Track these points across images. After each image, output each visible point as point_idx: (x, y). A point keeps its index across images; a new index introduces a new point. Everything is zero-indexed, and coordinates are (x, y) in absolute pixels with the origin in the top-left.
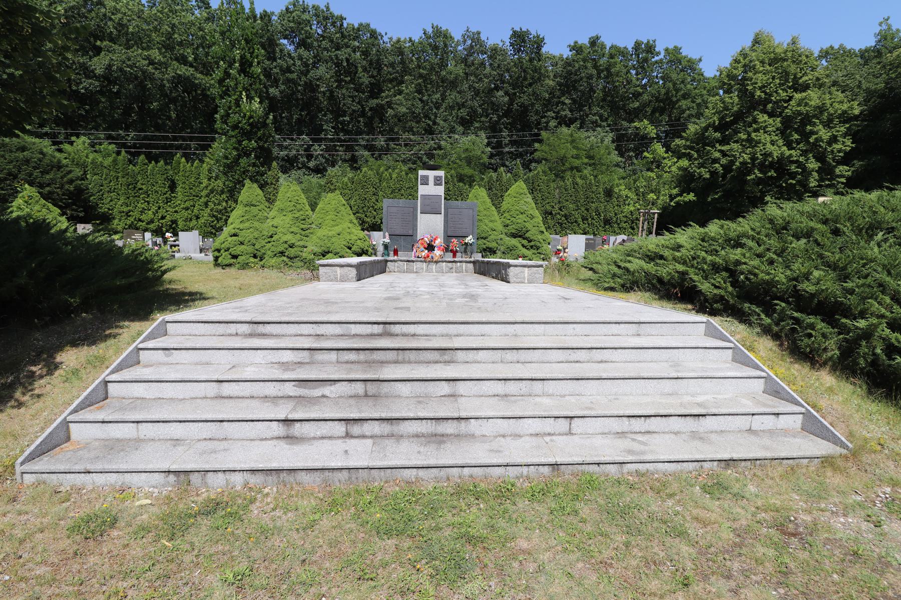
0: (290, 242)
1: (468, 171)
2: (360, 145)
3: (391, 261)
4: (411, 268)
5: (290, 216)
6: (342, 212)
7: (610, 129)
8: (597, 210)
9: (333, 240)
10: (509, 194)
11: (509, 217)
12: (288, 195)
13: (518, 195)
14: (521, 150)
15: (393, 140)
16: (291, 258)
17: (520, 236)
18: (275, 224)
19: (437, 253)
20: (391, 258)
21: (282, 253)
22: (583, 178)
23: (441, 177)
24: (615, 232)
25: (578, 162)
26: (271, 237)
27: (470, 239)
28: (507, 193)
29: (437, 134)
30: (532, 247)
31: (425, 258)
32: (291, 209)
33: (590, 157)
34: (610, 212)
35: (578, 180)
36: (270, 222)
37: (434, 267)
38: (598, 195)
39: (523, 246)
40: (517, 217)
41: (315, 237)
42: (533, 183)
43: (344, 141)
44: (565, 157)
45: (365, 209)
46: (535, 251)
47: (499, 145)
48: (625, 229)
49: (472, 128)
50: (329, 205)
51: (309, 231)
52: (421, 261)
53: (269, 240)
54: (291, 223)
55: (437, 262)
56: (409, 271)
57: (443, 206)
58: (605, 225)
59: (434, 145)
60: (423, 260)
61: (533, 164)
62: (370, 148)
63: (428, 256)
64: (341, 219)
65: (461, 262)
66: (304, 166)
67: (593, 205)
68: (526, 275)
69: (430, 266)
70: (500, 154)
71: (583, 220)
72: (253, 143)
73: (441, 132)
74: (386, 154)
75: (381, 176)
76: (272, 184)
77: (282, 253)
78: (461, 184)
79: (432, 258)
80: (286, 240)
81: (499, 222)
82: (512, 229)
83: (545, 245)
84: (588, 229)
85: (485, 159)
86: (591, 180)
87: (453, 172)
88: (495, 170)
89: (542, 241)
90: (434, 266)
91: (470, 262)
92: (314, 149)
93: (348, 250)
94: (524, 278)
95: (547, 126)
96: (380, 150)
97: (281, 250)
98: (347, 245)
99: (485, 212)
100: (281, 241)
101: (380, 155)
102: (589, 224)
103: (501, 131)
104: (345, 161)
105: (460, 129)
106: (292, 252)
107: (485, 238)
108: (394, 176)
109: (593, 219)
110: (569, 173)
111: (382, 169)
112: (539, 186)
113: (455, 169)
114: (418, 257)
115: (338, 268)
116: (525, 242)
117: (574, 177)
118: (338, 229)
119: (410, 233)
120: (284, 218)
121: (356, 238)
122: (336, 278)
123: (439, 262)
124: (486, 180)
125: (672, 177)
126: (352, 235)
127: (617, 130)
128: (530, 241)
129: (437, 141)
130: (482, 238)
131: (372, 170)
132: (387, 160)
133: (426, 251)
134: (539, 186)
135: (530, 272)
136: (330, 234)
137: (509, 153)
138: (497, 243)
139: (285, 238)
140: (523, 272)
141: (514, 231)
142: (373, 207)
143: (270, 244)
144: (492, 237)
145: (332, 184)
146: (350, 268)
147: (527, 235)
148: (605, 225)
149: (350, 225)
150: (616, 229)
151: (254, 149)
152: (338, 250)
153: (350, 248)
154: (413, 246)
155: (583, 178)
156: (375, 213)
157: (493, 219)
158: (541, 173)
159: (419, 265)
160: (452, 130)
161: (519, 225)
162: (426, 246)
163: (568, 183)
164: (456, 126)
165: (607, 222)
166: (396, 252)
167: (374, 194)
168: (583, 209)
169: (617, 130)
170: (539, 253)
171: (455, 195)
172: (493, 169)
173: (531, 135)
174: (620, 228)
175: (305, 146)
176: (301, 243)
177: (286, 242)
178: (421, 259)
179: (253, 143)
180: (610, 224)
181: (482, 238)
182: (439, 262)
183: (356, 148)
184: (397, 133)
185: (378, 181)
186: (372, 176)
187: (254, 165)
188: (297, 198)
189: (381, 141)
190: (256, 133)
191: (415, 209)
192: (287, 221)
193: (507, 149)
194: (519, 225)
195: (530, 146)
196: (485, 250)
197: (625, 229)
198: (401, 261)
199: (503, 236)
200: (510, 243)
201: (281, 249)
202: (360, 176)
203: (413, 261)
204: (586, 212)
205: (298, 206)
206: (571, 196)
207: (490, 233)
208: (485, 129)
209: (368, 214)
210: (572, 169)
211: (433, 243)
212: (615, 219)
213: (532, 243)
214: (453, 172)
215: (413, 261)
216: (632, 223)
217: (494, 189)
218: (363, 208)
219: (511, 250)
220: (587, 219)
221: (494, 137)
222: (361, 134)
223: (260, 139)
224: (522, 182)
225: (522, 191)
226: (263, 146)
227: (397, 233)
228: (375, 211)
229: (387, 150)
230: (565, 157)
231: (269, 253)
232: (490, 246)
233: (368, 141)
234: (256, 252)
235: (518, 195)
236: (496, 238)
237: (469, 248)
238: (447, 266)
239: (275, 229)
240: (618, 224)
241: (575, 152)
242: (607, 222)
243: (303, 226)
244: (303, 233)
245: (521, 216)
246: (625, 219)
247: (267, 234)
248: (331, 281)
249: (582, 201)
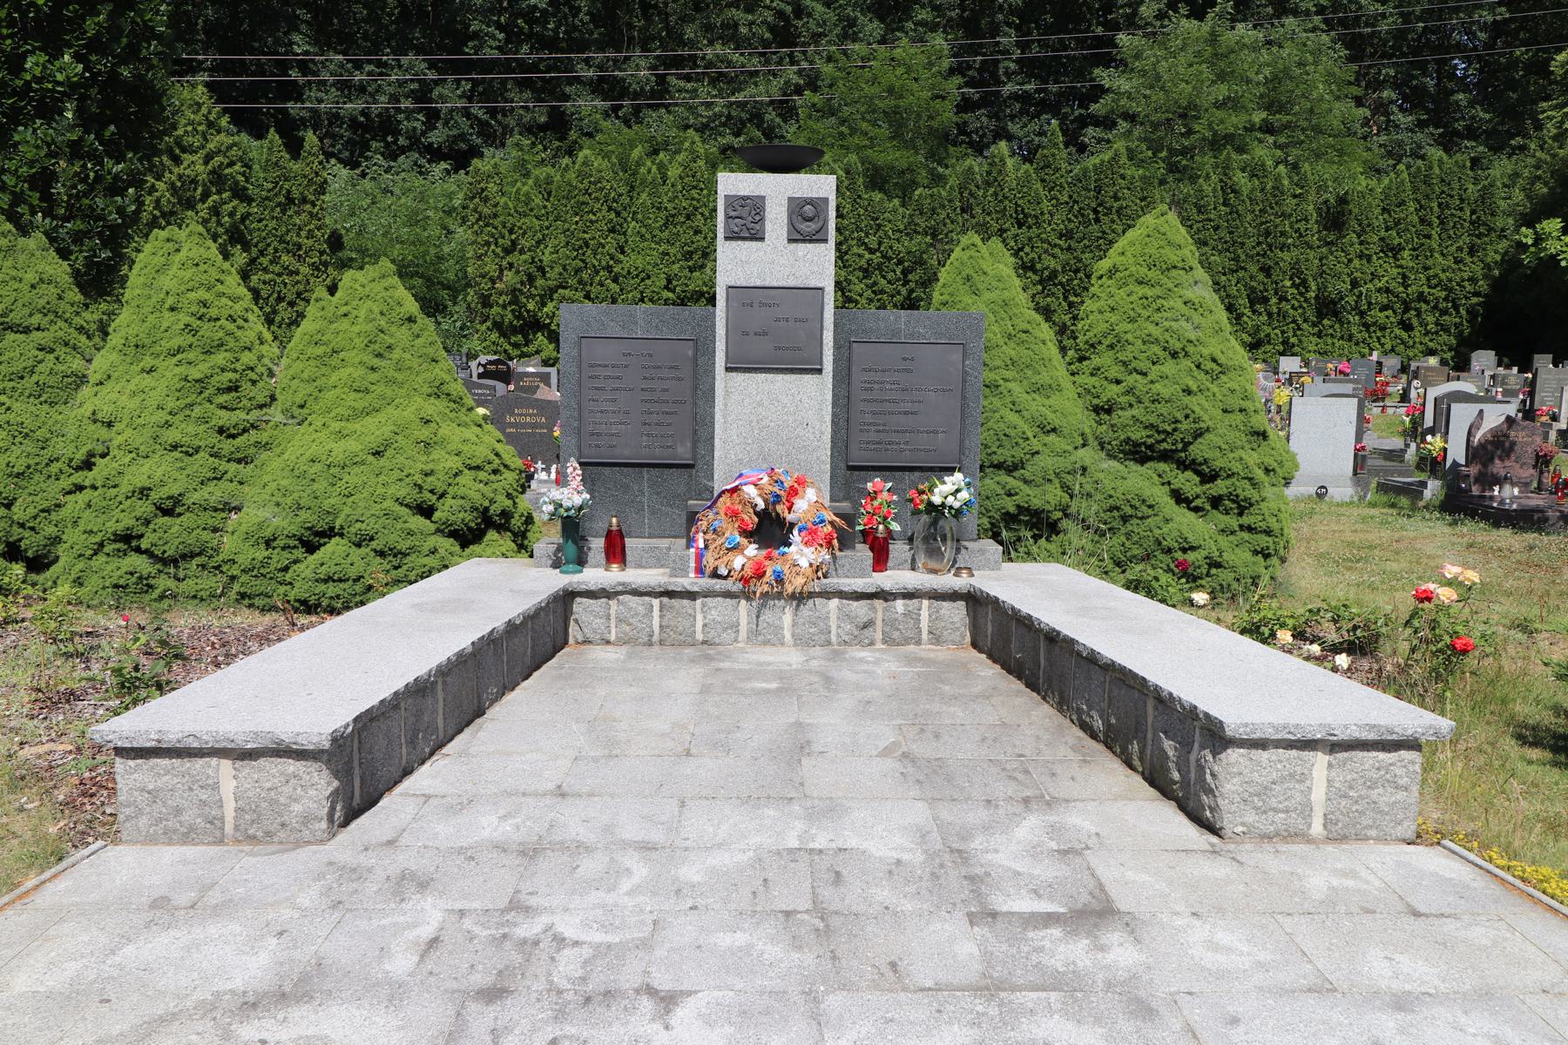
0: (164, 492)
1: (892, 156)
2: (578, 80)
3: (591, 594)
4: (683, 624)
5: (170, 371)
6: (396, 354)
7: (1326, 21)
8: (1296, 272)
9: (353, 477)
10: (1112, 272)
11: (1115, 371)
12: (166, 282)
13: (1153, 275)
14: (1053, 88)
15: (677, 62)
16: (165, 561)
17: (1165, 456)
18: (105, 412)
19: (802, 554)
20: (595, 575)
21: (128, 540)
22: (1256, 171)
23: (819, 204)
24: (1350, 338)
25: (1234, 119)
26: (88, 465)
27: (950, 489)
28: (1104, 265)
29: (804, 44)
30: (1216, 502)
31: (745, 580)
32: (177, 342)
33: (1272, 106)
34: (1338, 276)
35: (1241, 179)
36: (88, 400)
37: (788, 618)
38: (1302, 226)
39: (1178, 497)
40: (1155, 372)
41: (276, 464)
42: (1098, 190)
43: (534, 68)
44: (1192, 106)
45: (585, 276)
46: (1233, 521)
47: (988, 76)
48: (1383, 328)
49: (910, 25)
50: (344, 324)
51: (253, 436)
52: (728, 595)
53: (78, 478)
54: (171, 404)
55: (800, 598)
56: (673, 640)
57: (828, 337)
58: (1321, 315)
59: (795, 79)
60: (737, 587)
61: (1091, 131)
62: (608, 88)
63: (760, 574)
64: (391, 382)
65: (909, 595)
66: (415, 143)
67: (1286, 256)
68: (1318, 794)
69: (767, 616)
70: (991, 102)
71: (1252, 303)
72: (68, 66)
73: (816, 38)
74: (655, 107)
75: (634, 174)
76: (304, 200)
77: (128, 540)
78: (878, 196)
79: (779, 580)
80: (141, 481)
81: (1070, 392)
82: (1130, 423)
83: (1268, 492)
84: (1267, 329)
85: (947, 115)
86: (1278, 178)
87: (853, 157)
88: (979, 149)
89: (1259, 474)
90: (785, 617)
91: (953, 596)
92: (441, 96)
93: (418, 522)
94: (1306, 810)
95: (1135, 13)
96: (636, 96)
97: (120, 527)
98: (410, 494)
99: (1010, 351)
100: (125, 488)
101: (637, 110)
102: (1270, 315)
103: (995, 31)
104: (531, 129)
105: (873, 27)
106: (171, 534)
107: (1011, 468)
108: (673, 172)
109: (1283, 299)
110: (1206, 161)
111: (636, 153)
112: (1116, 198)
113: (859, 148)
114: (715, 575)
115: (226, 765)
116: (1188, 482)
117: (1226, 169)
118: (374, 429)
119: (683, 452)
120: (148, 380)
121: (454, 463)
122: (216, 822)
123: (811, 595)
124: (953, 181)
125: (1538, 167)
126: (437, 453)
127: (1343, 23)
128: (1209, 477)
129: (805, 65)
130: (998, 466)
131: (607, 156)
132: (659, 123)
133: (752, 550)
134: (1116, 198)
135: (1340, 777)
136: (340, 449)
137: (1015, 97)
138: (1066, 488)
139: (139, 475)
140: (1304, 778)
141: (1138, 435)
142: (609, 268)
143: (81, 498)
144: (1046, 462)
145: (486, 200)
146: (291, 766)
147: (1198, 450)
148: (1321, 315)
149: (433, 408)
150: (1354, 330)
151: (72, 87)
152: (369, 526)
153: (426, 511)
154: (692, 518)
155: (1256, 171)
156: (615, 287)
157: (1044, 378)
158: (1124, 159)
159: (718, 609)
160: (849, 31)
161: (1163, 409)
162: (751, 520)
163: (1207, 189)
164: (861, 19)
165: (1328, 307)
166: (615, 552)
167: (612, 230)
168: (1253, 269)
169: (1343, 23)
170: (1250, 529)
171: (859, 229)
172: (971, 144)
173: (1081, 43)
174: (1366, 326)
175: (415, 86)
176: (214, 493)
177: (144, 492)
178: (728, 585)
179: (68, 66)
180: (1336, 314)
181: (998, 466)
182: (811, 595)
183: (568, 89)
184: (692, 44)
185: (623, 190)
186: (608, 175)
187: (76, 150)
188: (202, 294)
189: (639, 70)
190: (77, 22)
191: (703, 347)
192: (154, 398)
193: (1009, 88)
194: (1163, 409)
195: (1080, 74)
196: (1010, 519)
197: (1383, 328)
198: (636, 593)
199: (1087, 456)
200: (1123, 486)
201: (123, 520)
202: (571, 175)
203: (692, 596)
204: (1261, 277)
205: (206, 329)
206: (1216, 228)
207: (1036, 444)
208: (949, 26)
209: (595, 290)
210: (1217, 143)
211: (781, 508)
212: (1351, 299)
213: (1220, 487)
214: (853, 157)
215: (692, 596)
216: (1406, 310)
217: (978, 210)
218: (578, 271)
219: (1125, 519)
220: (1266, 300)
221: (974, 50)
222: (582, 47)
223: (95, 45)
224: (1172, 217)
225: (1173, 256)
226: (113, 75)
227: (625, 453)
228: (615, 280)
229: (659, 94)
230: (1192, 106)
231: (72, 536)
232: (1036, 503)
233: (601, 68)
234: (17, 532)
235: (1153, 275)
236: (1063, 463)
237: (947, 524)
238: (846, 616)
239: (103, 433)
240: (1362, 314)
241: (1222, 91)
242: (1328, 307)
243: (225, 418)
244: (227, 446)
245: (1169, 367)
246: (1383, 299)
247: (68, 451)
248: (188, 837)
249: (1250, 243)
